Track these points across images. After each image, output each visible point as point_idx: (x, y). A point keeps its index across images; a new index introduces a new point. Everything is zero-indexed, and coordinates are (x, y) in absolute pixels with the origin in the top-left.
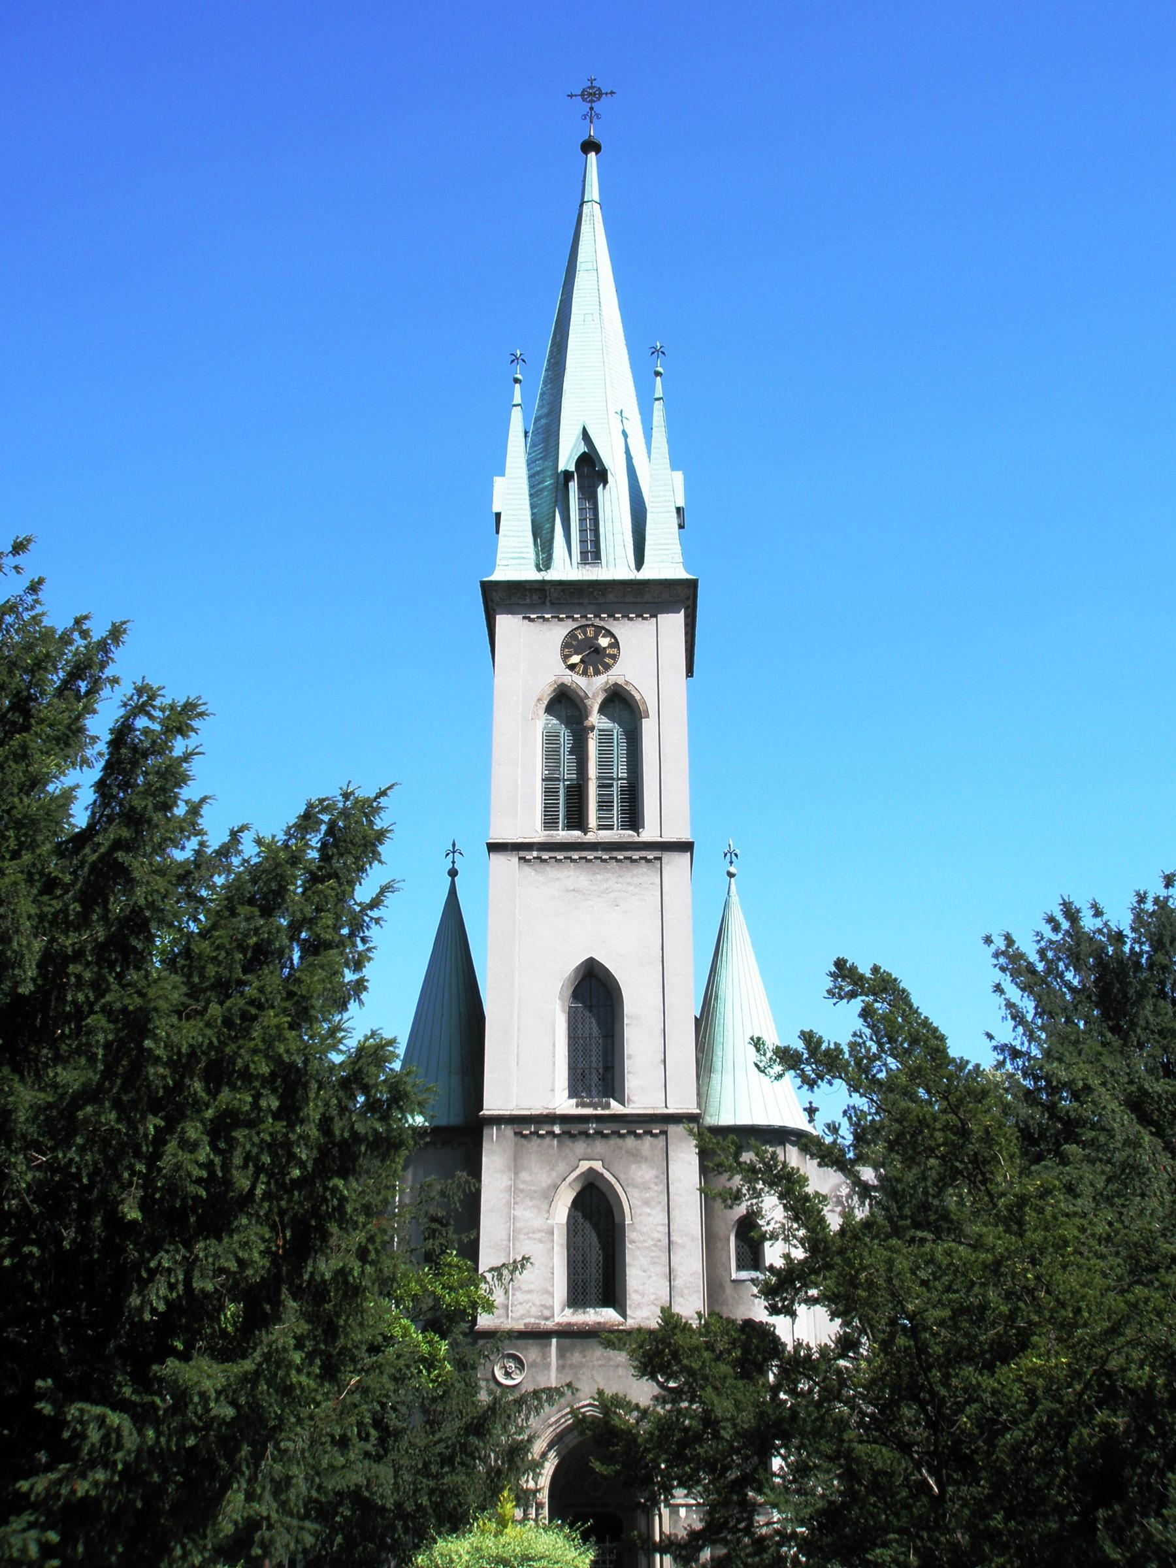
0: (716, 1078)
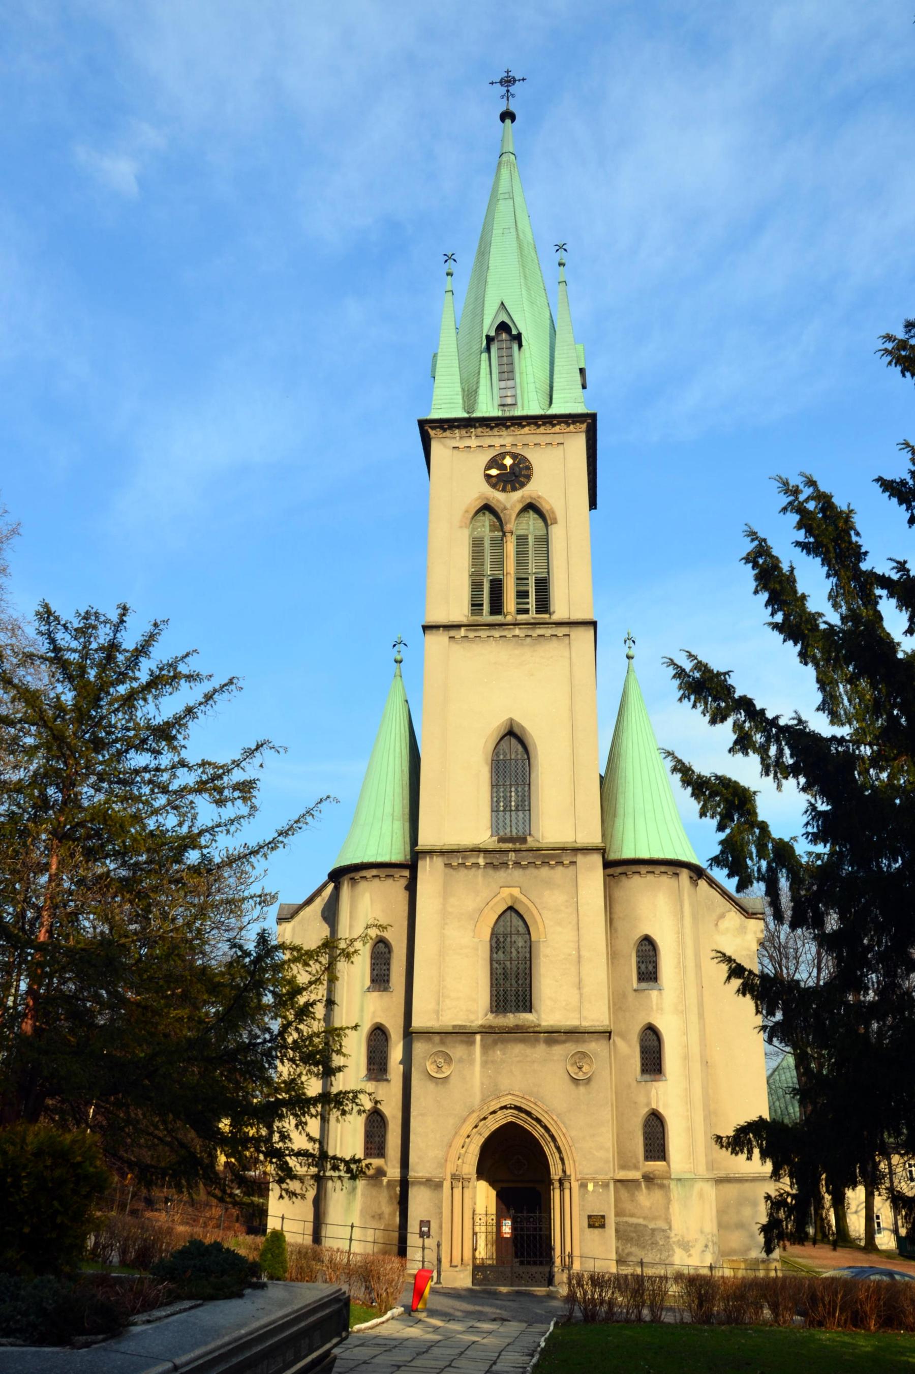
0: (619, 822)
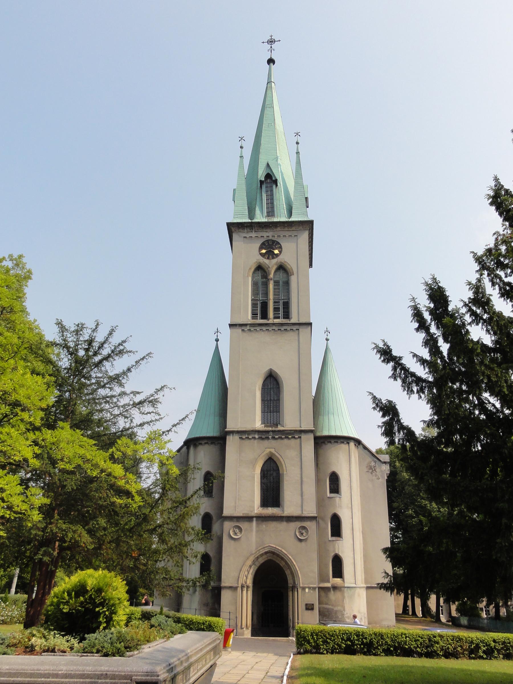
0: (321, 418)
